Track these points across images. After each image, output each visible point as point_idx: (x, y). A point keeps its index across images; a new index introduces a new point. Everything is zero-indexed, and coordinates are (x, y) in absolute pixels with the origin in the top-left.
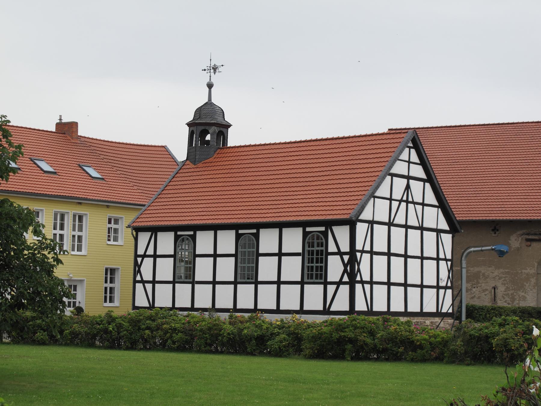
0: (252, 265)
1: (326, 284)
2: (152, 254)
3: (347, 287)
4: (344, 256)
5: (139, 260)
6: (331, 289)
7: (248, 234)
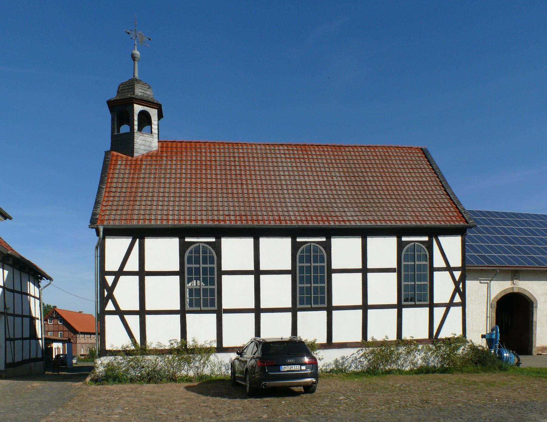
0: (425, 263)
1: (432, 306)
2: (435, 309)
3: (107, 269)
4: (454, 272)
5: (457, 299)
6: (439, 313)
7: (311, 242)
